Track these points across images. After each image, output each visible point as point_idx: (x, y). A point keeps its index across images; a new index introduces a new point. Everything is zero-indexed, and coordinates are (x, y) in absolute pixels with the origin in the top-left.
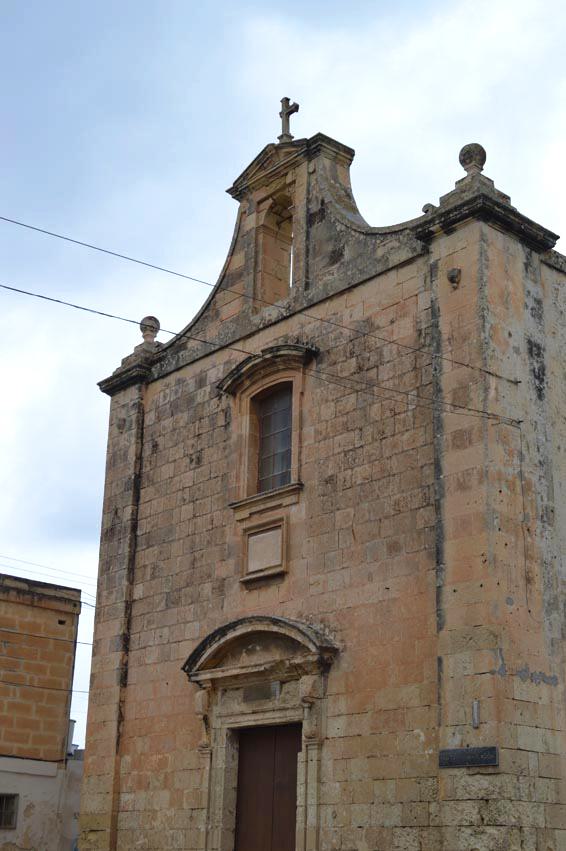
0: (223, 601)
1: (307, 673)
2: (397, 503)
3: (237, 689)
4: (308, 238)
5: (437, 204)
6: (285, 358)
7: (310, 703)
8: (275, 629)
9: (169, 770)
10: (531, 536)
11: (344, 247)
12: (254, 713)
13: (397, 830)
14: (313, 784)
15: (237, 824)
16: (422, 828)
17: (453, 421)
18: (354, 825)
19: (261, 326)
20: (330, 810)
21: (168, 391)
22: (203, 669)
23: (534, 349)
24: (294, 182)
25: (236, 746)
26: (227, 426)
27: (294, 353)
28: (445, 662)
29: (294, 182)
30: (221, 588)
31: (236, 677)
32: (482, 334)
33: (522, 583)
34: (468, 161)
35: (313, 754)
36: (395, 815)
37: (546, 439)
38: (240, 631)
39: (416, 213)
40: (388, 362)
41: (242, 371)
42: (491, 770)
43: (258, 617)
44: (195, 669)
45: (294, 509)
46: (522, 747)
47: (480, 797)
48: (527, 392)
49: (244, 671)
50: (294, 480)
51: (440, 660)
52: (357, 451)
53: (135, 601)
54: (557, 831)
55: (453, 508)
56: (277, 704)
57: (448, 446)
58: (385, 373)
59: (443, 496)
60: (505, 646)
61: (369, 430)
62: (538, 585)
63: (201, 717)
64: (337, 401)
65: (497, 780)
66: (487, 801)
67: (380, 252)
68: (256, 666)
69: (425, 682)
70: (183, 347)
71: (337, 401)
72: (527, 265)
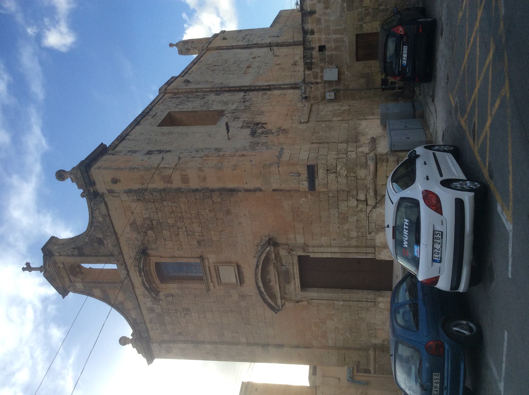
0: (248, 295)
1: (279, 253)
2: (210, 211)
3: (285, 287)
4: (91, 256)
5: (81, 191)
6: (144, 265)
7: (290, 250)
8: (260, 267)
10: (226, 155)
11: (96, 237)
12: (294, 279)
13: (339, 211)
14: (322, 250)
15: (339, 288)
16: (338, 200)
17: (177, 183)
19: (129, 279)
20: (332, 242)
21: (155, 328)
22: (277, 304)
23: (150, 153)
24: (63, 263)
25: (308, 288)
26: (172, 295)
27: (142, 260)
28: (274, 188)
29: (63, 263)
30: (243, 297)
31: (280, 287)
32: (141, 169)
33: (244, 157)
34: (63, 177)
35: (311, 249)
36: (334, 212)
37: (188, 150)
38: (261, 285)
39: (84, 201)
40: (150, 215)
41: (148, 287)
42: (316, 168)
43: (255, 275)
44: (276, 307)
45: (210, 260)
46: (307, 158)
47: (326, 173)
48: (167, 156)
49: (277, 283)
50: (198, 261)
51: (274, 190)
52: (187, 230)
54: (338, 148)
55: (213, 183)
56: (290, 267)
57: (188, 186)
59: (208, 188)
60: (268, 162)
61: (179, 224)
62: (245, 153)
63: (296, 304)
64: (165, 240)
65: (319, 166)
66: (328, 170)
67: (101, 219)
68: (275, 277)
69: (282, 198)
70: (135, 320)
71: (165, 240)
72: (113, 154)
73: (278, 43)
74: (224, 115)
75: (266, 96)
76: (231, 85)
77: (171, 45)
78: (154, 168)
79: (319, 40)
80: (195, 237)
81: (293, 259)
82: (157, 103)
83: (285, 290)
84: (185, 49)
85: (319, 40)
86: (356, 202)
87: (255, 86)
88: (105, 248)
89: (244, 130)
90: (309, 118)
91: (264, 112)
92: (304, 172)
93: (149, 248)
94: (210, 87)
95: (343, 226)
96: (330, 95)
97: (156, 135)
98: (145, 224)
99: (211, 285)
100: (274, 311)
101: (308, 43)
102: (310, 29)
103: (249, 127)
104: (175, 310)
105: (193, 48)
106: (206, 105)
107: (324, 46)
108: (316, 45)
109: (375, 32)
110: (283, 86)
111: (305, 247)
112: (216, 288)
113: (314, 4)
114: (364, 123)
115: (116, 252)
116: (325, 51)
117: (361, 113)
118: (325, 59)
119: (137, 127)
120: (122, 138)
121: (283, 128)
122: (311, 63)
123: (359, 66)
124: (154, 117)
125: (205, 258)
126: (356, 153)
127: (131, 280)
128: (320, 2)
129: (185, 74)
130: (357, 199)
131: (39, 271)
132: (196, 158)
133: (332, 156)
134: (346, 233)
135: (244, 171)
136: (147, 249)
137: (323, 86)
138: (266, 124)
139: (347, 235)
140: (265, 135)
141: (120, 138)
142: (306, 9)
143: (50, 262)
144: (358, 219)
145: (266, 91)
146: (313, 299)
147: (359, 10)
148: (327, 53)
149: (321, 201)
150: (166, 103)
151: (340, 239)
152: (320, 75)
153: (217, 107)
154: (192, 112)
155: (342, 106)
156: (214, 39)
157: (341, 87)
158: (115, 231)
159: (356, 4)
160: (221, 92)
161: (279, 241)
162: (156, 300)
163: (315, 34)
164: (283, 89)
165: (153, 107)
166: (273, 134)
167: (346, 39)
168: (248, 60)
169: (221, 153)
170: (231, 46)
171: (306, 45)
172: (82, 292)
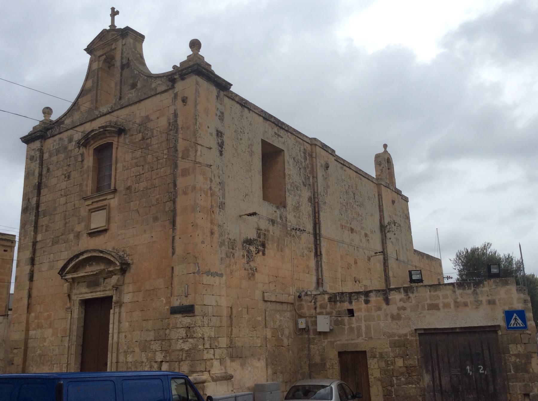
1: (115, 274)
3: (84, 282)
4: (121, 75)
6: (110, 131)
7: (116, 288)
8: (101, 255)
9: (52, 319)
11: (138, 81)
12: (91, 292)
14: (116, 324)
16: (163, 340)
17: (182, 164)
18: (134, 341)
19: (99, 116)
20: (124, 334)
21: (55, 143)
23: (219, 134)
24: (115, 48)
25: (83, 307)
26: (82, 161)
27: (114, 129)
29: (115, 48)
30: (78, 236)
33: (209, 234)
36: (151, 336)
38: (85, 256)
40: (156, 136)
42: (191, 315)
45: (112, 200)
50: (112, 187)
51: (173, 268)
52: (141, 175)
53: (37, 242)
56: (102, 288)
58: (154, 141)
59: (176, 197)
61: (146, 167)
62: (216, 235)
67: (153, 86)
68: (92, 272)
71: (133, 152)
73: (387, 260)
74: (279, 209)
75: (306, 252)
76: (321, 214)
77: (385, 146)
78: (196, 140)
79: (360, 310)
80: (134, 183)
81: (109, 290)
82: (297, 137)
83: (82, 282)
84: (380, 161)
85: (360, 310)
86: (160, 360)
87: (320, 240)
88: (128, 90)
89: (255, 232)
90: (271, 301)
91: (282, 251)
92: (188, 301)
93: (126, 136)
94: (319, 191)
95: (138, 346)
96: (302, 323)
97: (249, 139)
98: (147, 131)
99: (90, 202)
100: (60, 271)
101: (356, 297)
102: (370, 299)
103: (259, 237)
104: (70, 164)
105: (382, 169)
106: (294, 188)
107: (353, 316)
108: (354, 306)
109: (369, 372)
110: (320, 269)
111: (120, 304)
112: (87, 207)
113: (396, 303)
114: (261, 364)
115: (123, 101)
116: (349, 316)
117: (277, 360)
118: (340, 316)
119: (261, 119)
120: (244, 104)
121: (256, 273)
122: (335, 302)
123: (333, 355)
124: (276, 136)
125: (114, 196)
126: (212, 359)
127: (98, 118)
128: (398, 310)
129: (341, 164)
130: (163, 361)
131: (110, 24)
132: (210, 183)
133: (208, 332)
134: (131, 349)
135: (191, 236)
136: (126, 134)
137: (312, 315)
138: (264, 254)
139: (129, 350)
140: (245, 255)
141: (245, 102)
142: (390, 294)
143: (116, 36)
144: (144, 364)
145: (314, 251)
146: (71, 313)
147: (391, 354)
148: (346, 319)
149: (162, 321)
150: (298, 146)
151: (126, 343)
152: (324, 311)
153: (290, 201)
154: (284, 174)
155: (288, 338)
156: (393, 191)
157: (312, 336)
158: (142, 100)
159: (397, 350)
160: (313, 202)
161: (127, 274)
162: (79, 144)
163: (366, 305)
164: (317, 270)
165: (292, 133)
166: (248, 263)
167: (360, 340)
168: (362, 228)
169: (217, 210)
170: (383, 209)
171: (354, 296)
172: (90, 67)
